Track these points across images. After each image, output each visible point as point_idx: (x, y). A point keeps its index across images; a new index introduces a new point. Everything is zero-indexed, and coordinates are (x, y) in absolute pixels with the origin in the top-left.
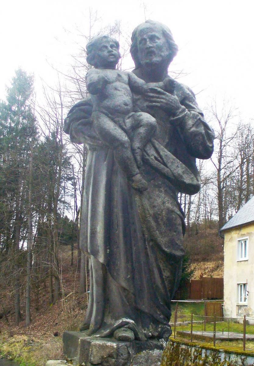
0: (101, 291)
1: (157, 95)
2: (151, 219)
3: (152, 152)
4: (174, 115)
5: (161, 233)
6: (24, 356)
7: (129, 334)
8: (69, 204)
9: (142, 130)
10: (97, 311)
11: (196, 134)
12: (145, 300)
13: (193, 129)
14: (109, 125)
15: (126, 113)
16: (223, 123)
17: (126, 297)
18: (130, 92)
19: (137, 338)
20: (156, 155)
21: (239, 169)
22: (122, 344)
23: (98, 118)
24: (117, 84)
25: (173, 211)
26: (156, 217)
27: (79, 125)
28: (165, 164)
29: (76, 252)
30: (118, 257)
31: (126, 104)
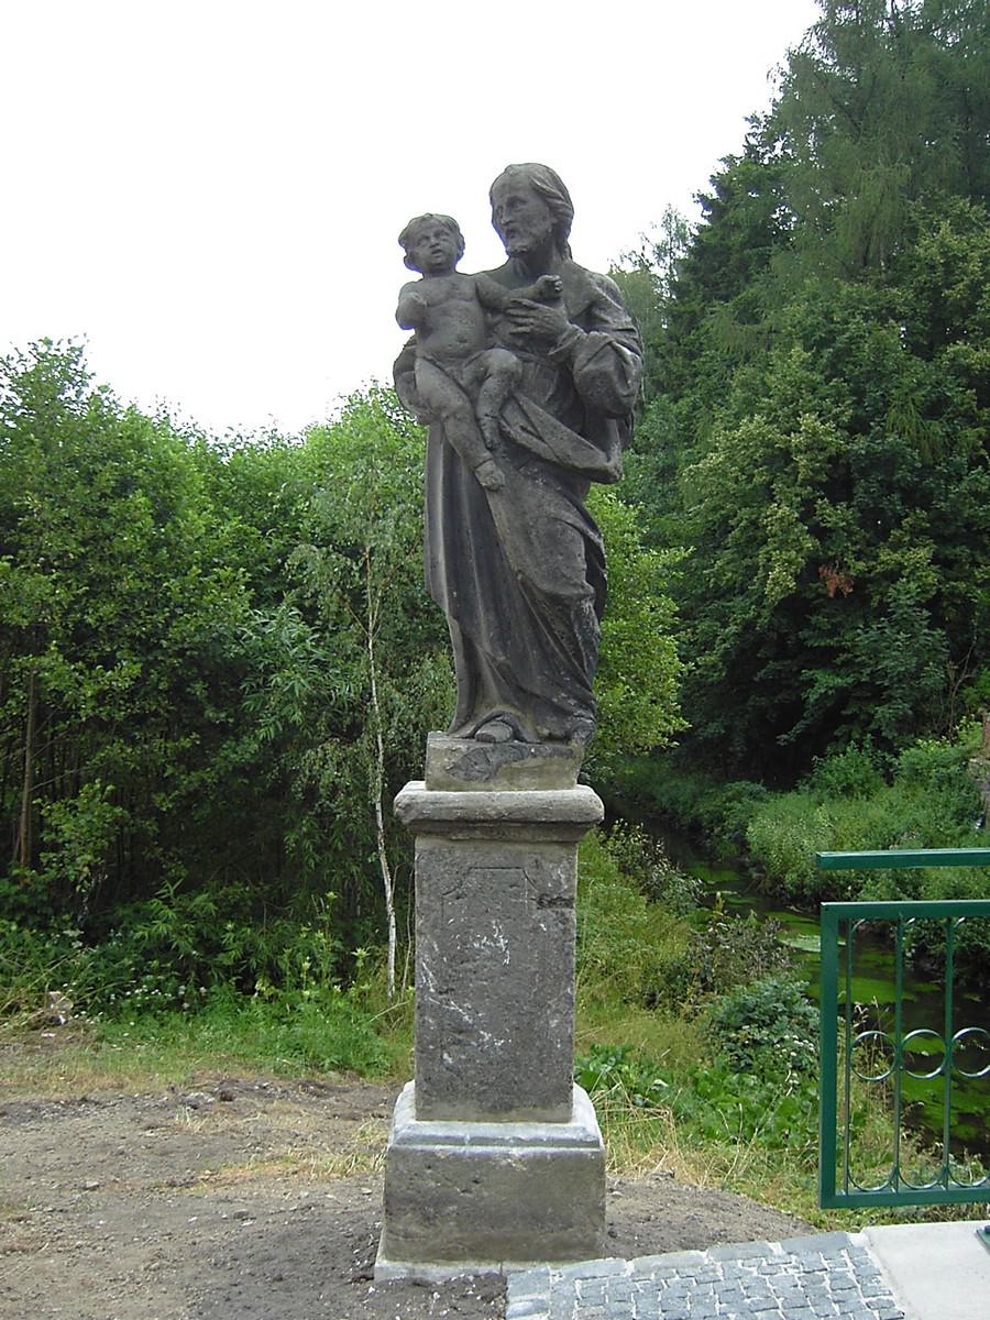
1: (524, 313)
4: (553, 344)
9: (491, 384)
13: (591, 367)
20: (523, 423)
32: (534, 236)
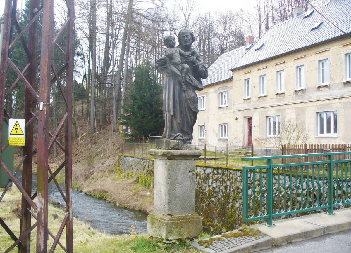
0: (170, 125)
2: (188, 100)
3: (188, 77)
4: (195, 64)
5: (191, 105)
6: (59, 176)
7: (181, 138)
8: (80, 72)
9: (185, 70)
10: (169, 131)
11: (202, 71)
12: (185, 127)
13: (201, 69)
14: (174, 69)
15: (179, 64)
16: (187, 16)
17: (179, 126)
18: (180, 56)
19: (183, 140)
21: (198, 47)
22: (180, 141)
23: (170, 66)
24: (176, 54)
25: (195, 97)
26: (189, 99)
27: (162, 68)
28: (192, 82)
29: (85, 106)
31: (179, 62)
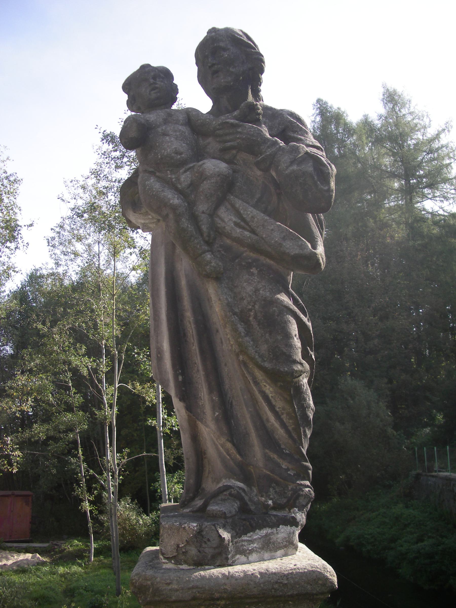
9: (206, 186)
15: (183, 163)
30: (200, 386)
32: (228, 301)
